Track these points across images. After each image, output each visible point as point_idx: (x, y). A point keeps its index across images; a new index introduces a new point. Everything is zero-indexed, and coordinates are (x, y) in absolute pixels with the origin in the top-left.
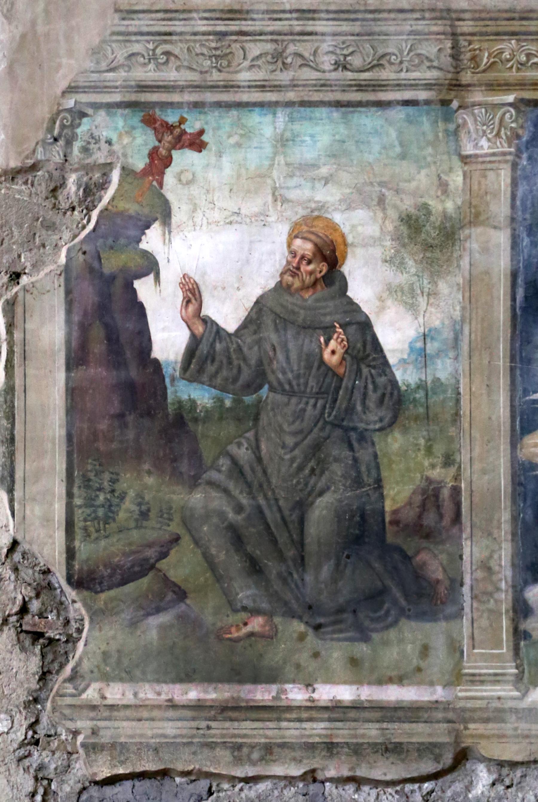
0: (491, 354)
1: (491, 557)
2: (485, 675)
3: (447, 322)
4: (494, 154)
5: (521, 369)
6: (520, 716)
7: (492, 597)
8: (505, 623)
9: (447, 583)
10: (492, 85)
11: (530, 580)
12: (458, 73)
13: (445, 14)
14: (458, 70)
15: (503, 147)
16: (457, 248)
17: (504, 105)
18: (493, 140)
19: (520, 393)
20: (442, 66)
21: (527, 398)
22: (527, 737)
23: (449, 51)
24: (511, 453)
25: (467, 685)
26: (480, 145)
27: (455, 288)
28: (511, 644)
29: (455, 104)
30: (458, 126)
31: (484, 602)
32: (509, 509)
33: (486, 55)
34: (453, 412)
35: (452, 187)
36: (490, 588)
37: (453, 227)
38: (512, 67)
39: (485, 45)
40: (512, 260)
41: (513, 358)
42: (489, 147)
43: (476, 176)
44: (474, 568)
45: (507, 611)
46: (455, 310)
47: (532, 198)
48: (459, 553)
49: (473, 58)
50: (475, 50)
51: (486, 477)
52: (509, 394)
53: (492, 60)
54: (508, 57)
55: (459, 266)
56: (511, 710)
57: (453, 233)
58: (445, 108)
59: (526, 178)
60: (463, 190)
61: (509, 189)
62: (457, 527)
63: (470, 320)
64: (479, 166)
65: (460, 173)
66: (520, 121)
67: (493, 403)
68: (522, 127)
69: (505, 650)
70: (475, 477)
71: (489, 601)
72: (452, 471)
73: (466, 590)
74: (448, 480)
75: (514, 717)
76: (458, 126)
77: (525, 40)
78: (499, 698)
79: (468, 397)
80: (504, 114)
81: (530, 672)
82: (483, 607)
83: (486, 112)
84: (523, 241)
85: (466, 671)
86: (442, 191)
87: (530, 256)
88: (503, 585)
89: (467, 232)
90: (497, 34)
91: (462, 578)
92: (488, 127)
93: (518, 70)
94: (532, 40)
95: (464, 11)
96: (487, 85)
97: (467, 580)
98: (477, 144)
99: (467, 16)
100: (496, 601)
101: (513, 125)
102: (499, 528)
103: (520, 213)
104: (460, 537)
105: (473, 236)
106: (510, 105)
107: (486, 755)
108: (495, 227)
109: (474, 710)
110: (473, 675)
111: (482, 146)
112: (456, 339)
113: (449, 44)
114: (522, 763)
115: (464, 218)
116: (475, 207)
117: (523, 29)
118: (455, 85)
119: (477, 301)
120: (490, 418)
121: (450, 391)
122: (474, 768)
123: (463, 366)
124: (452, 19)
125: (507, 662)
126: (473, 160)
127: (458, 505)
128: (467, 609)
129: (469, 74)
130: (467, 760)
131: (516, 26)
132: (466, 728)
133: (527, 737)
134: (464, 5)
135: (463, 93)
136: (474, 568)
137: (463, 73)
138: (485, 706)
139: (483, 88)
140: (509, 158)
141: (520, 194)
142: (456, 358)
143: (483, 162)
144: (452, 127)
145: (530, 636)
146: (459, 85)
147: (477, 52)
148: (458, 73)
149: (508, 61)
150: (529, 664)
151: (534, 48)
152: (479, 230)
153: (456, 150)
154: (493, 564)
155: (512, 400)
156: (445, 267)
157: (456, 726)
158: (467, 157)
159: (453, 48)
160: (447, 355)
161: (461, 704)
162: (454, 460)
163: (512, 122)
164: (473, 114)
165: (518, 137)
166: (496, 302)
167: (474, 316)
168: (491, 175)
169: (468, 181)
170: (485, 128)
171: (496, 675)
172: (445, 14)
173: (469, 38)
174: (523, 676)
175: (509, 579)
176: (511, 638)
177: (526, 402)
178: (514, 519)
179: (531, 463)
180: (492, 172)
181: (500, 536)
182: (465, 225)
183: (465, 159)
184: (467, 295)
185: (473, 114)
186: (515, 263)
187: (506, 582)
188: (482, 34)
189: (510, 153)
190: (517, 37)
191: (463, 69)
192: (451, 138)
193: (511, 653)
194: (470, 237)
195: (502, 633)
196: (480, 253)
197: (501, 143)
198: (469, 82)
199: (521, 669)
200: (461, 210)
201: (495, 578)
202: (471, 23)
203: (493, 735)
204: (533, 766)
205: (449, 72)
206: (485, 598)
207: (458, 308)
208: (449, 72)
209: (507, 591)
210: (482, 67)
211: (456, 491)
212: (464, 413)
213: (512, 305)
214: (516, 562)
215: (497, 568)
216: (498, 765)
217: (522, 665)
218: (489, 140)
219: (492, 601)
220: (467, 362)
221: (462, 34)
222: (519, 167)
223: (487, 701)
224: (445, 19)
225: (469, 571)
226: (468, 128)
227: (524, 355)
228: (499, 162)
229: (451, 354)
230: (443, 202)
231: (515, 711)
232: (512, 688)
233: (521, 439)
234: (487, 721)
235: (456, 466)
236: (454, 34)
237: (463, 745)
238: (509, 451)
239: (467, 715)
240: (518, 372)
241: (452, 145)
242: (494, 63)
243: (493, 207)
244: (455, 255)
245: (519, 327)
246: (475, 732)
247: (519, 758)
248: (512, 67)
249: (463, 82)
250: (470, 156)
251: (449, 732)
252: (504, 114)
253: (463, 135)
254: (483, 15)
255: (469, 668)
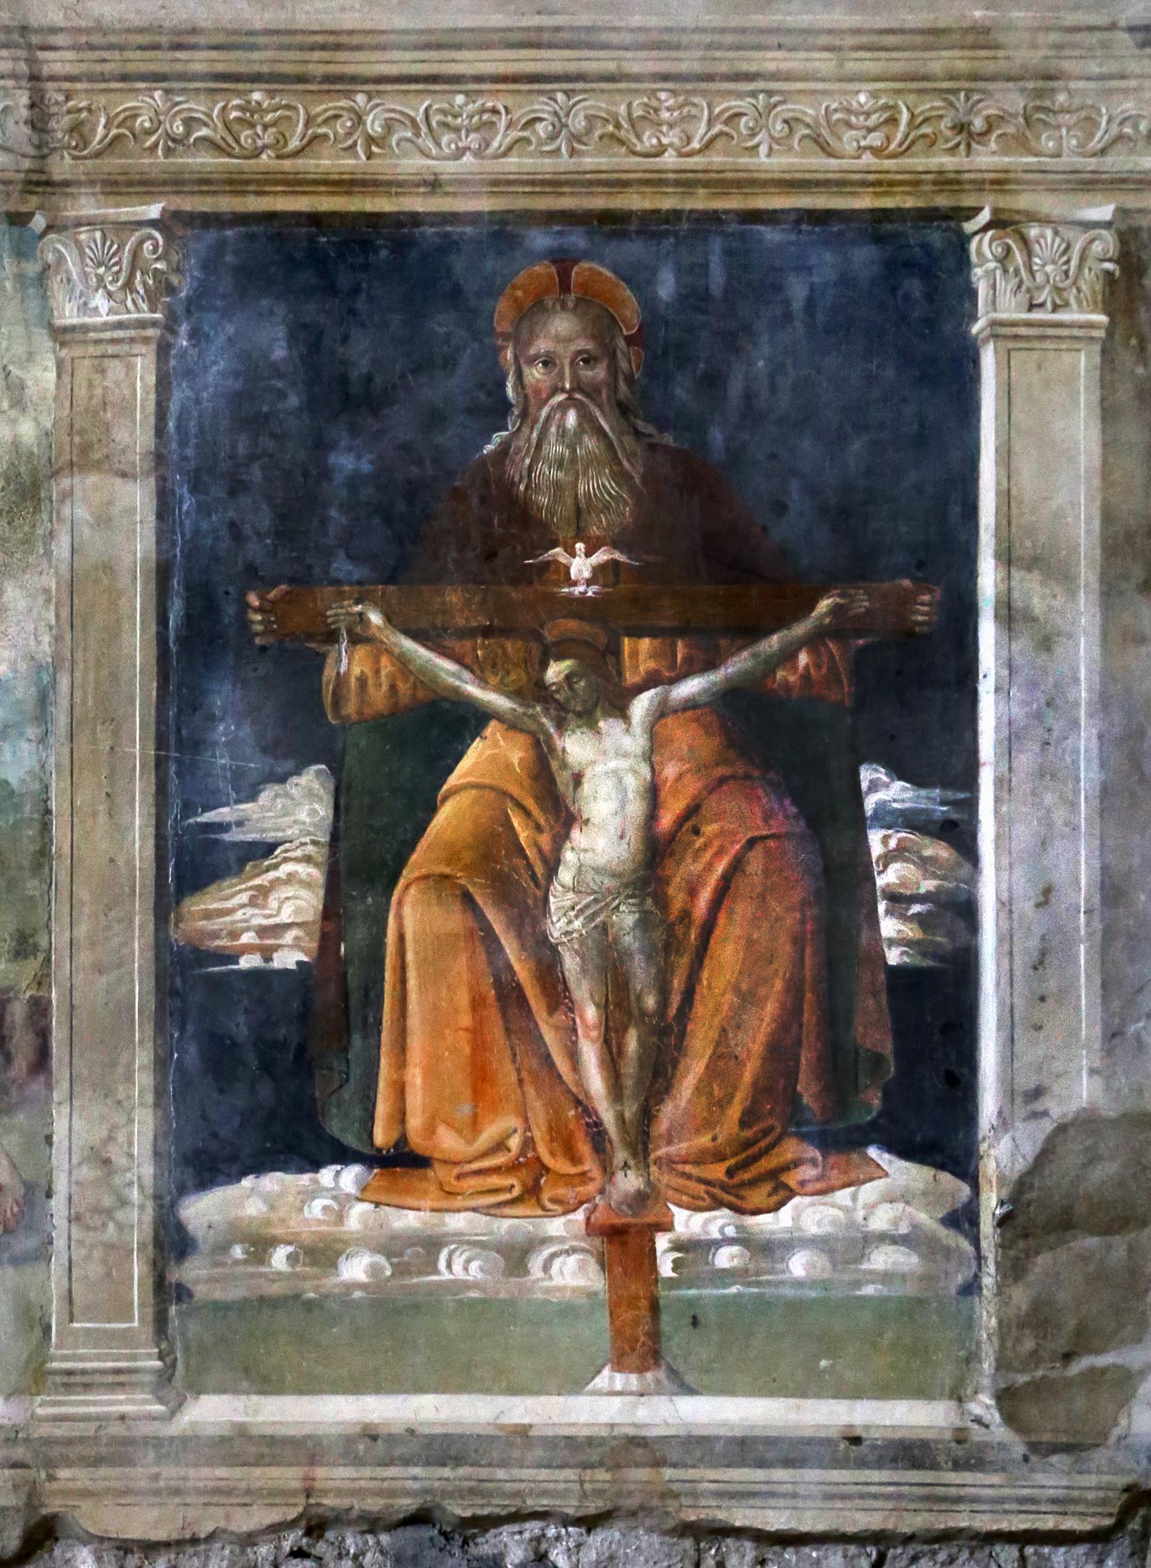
0: (116, 733)
1: (111, 1138)
2: (95, 1371)
3: (23, 667)
4: (120, 325)
5: (180, 762)
6: (164, 1451)
7: (113, 1219)
8: (138, 1269)
9: (20, 1191)
10: (115, 183)
11: (189, 1184)
12: (43, 157)
13: (16, 37)
14: (43, 151)
15: (138, 310)
16: (45, 516)
17: (140, 224)
18: (120, 296)
19: (176, 810)
20: (9, 144)
21: (191, 821)
22: (177, 1492)
23: (24, 113)
24: (157, 930)
25: (57, 1393)
26: (92, 305)
27: (41, 599)
28: (150, 1311)
29: (39, 222)
30: (47, 267)
31: (95, 1229)
32: (150, 1045)
33: (103, 121)
34: (33, 848)
35: (31, 392)
36: (107, 1201)
37: (34, 470)
38: (156, 145)
39: (102, 100)
40: (158, 542)
41: (161, 742)
42: (111, 311)
43: (84, 369)
44: (75, 1161)
45: (142, 1247)
46: (39, 643)
47: (200, 416)
48: (46, 1132)
49: (74, 129)
50: (80, 110)
51: (104, 980)
52: (153, 811)
53: (114, 132)
54: (147, 125)
55: (48, 554)
56: (146, 1441)
57: (36, 485)
58: (16, 230)
59: (188, 374)
60: (56, 398)
61: (152, 397)
62: (42, 1079)
63: (73, 662)
64: (91, 350)
65: (51, 364)
66: (175, 258)
67: (119, 831)
68: (178, 270)
69: (136, 1324)
70: (78, 980)
71: (104, 1225)
72: (32, 966)
73: (58, 1205)
74: (24, 985)
75: (152, 1455)
76: (47, 267)
77: (183, 91)
78: (122, 1417)
79: (67, 817)
80: (141, 243)
81: (187, 1365)
82: (91, 1238)
83: (104, 238)
84: (181, 502)
85: (55, 1365)
86: (11, 399)
87: (197, 532)
88: (135, 1195)
89: (65, 483)
90: (124, 78)
91: (50, 1182)
92: (108, 268)
93: (168, 152)
94: (197, 90)
95: (54, 30)
96: (104, 182)
97: (61, 1185)
98: (85, 304)
99: (59, 40)
100: (120, 1227)
101: (159, 266)
102: (129, 1078)
103: (174, 446)
104: (48, 1100)
105: (78, 494)
106: (153, 223)
107: (92, 1530)
108: (124, 475)
109: (69, 1442)
110: (70, 1373)
111: (96, 309)
112: (43, 700)
113: (24, 100)
114: (167, 1545)
115: (60, 454)
116: (81, 432)
117: (178, 67)
118: (38, 183)
119: (85, 627)
120: (112, 860)
121: (28, 808)
122: (69, 1555)
123: (57, 754)
124: (30, 47)
125: (143, 1347)
126: (79, 336)
127: (43, 1035)
128: (60, 1243)
129: (68, 160)
130: (57, 1540)
131: (160, 62)
132: (51, 1478)
133: (177, 1492)
134: (56, 17)
135: (54, 198)
136: (75, 1161)
137: (54, 159)
138: (91, 1433)
139: (98, 189)
140: (151, 332)
141: (174, 407)
142: (42, 740)
143: (98, 342)
144: (32, 268)
145: (190, 1295)
146: (48, 183)
147: (84, 114)
148: (43, 157)
149: (149, 133)
150: (187, 1349)
151: (202, 108)
152: (93, 479)
153: (41, 316)
154: (116, 1154)
155: (160, 824)
156: (18, 556)
157: (31, 1473)
158: (66, 330)
159: (32, 106)
160: (21, 734)
161: (45, 1430)
162: (36, 947)
163: (157, 259)
164: (78, 245)
165: (171, 290)
166: (126, 626)
167: (79, 656)
168: (115, 369)
169: (66, 379)
170: (102, 270)
171: (118, 1371)
172: (16, 37)
173: (66, 85)
174: (173, 1375)
175: (149, 1182)
176: (150, 1298)
177: (188, 830)
178: (161, 1064)
179: (196, 950)
180: (116, 362)
181: (129, 1097)
182: (61, 469)
183: (62, 335)
184: (65, 613)
185: (78, 245)
186: (164, 547)
187: (141, 1188)
188: (91, 78)
189: (154, 324)
190: (165, 85)
191: (55, 149)
192: (31, 291)
193: (150, 1329)
194: (70, 493)
195: (131, 1288)
196: (92, 527)
197: (133, 301)
198: (68, 177)
199: (168, 1360)
200: (53, 439)
201: (117, 1180)
202: (70, 55)
203: (108, 1491)
204: (190, 1550)
205: (24, 156)
206: (97, 1221)
207: (46, 639)
208: (24, 156)
209: (142, 1207)
210: (95, 145)
211: (39, 1009)
212: (59, 848)
213: (158, 633)
214: (164, 1147)
215: (123, 1161)
216: (119, 1548)
217: (172, 1351)
218: (110, 295)
219: (111, 1226)
220: (66, 751)
221: (52, 78)
222: (173, 352)
223: (98, 1423)
224: (17, 46)
225: (66, 1167)
226: (68, 272)
227: (184, 732)
228: (132, 340)
229: (32, 732)
230: (13, 422)
231: (157, 1442)
232: (150, 1397)
233: (178, 903)
234: (96, 1462)
235: (41, 956)
236: (34, 78)
237: (44, 1511)
238: (151, 927)
239: (56, 1452)
240: (173, 768)
241: (34, 305)
242: (118, 137)
243: (121, 435)
244: (40, 532)
245: (173, 679)
246: (70, 1484)
247: (161, 1535)
248: (156, 145)
249: (57, 177)
250: (73, 329)
251: (16, 1487)
252: (141, 243)
253: (55, 283)
254: (96, 39)
255: (65, 1358)
